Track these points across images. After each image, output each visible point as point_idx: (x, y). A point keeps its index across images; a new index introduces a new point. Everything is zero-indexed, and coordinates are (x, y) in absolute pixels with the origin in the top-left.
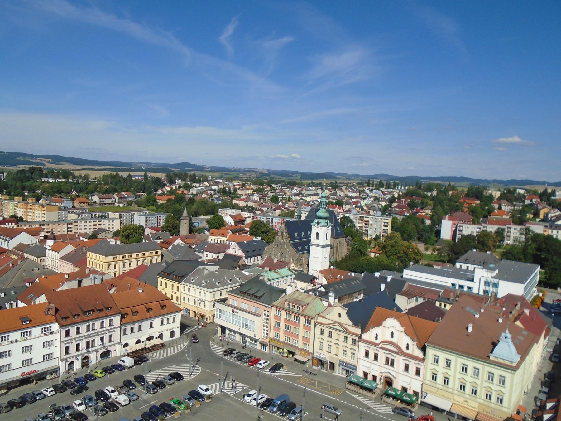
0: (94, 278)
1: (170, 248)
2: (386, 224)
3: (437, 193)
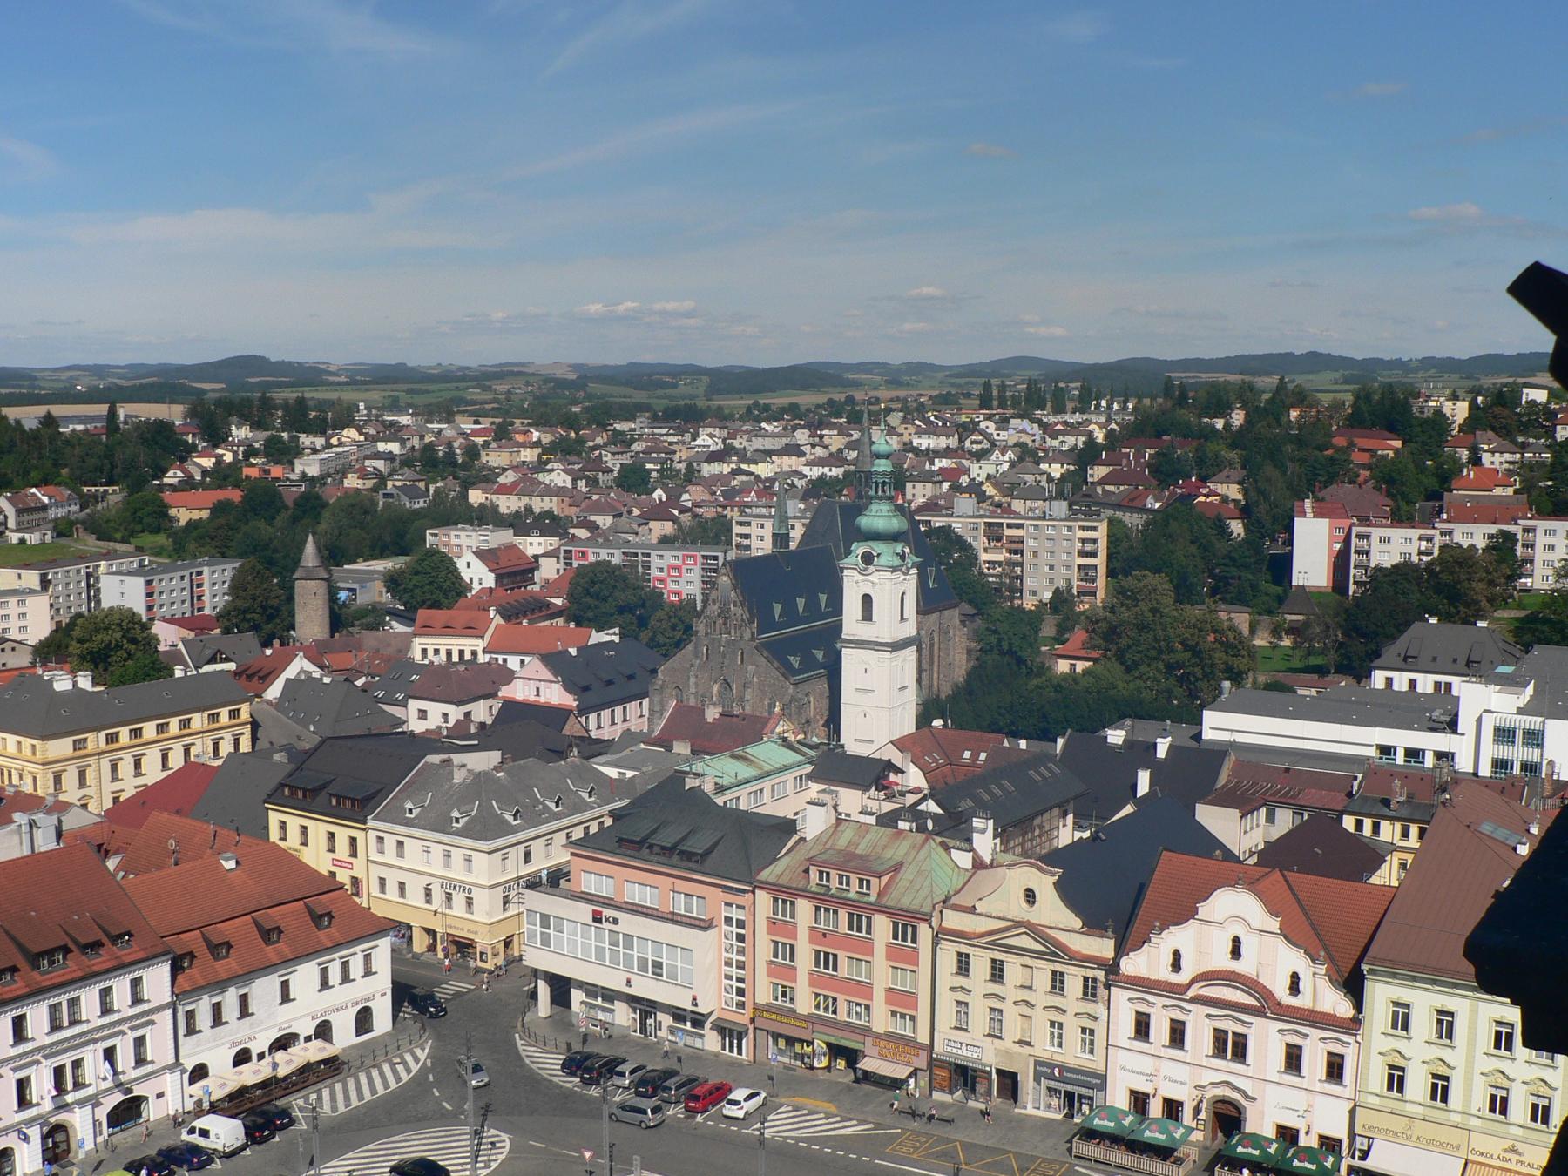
0: (32, 825)
1: (274, 691)
2: (1088, 547)
3: (1248, 420)
